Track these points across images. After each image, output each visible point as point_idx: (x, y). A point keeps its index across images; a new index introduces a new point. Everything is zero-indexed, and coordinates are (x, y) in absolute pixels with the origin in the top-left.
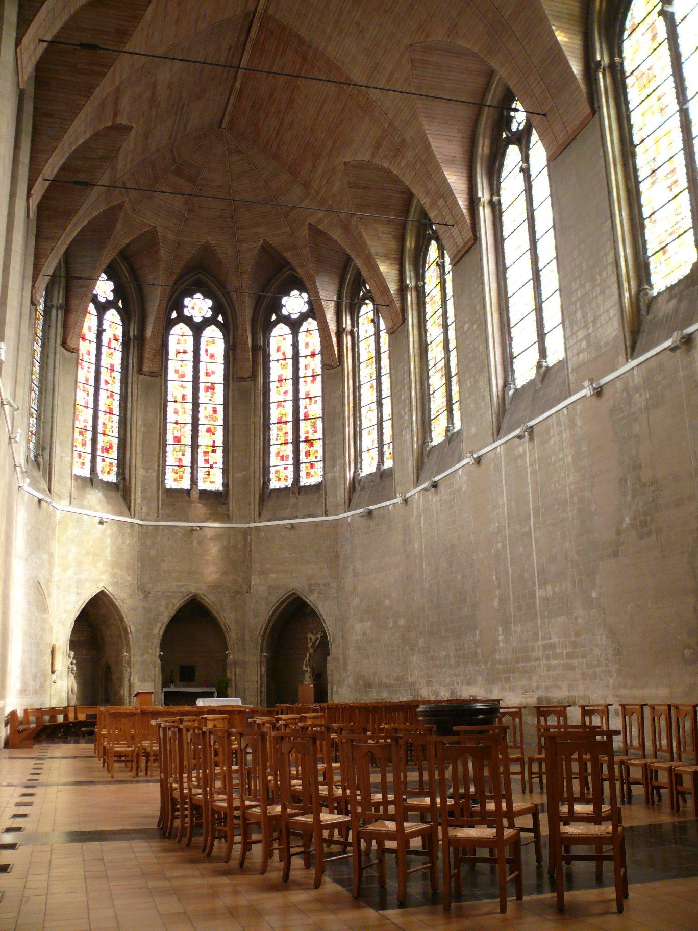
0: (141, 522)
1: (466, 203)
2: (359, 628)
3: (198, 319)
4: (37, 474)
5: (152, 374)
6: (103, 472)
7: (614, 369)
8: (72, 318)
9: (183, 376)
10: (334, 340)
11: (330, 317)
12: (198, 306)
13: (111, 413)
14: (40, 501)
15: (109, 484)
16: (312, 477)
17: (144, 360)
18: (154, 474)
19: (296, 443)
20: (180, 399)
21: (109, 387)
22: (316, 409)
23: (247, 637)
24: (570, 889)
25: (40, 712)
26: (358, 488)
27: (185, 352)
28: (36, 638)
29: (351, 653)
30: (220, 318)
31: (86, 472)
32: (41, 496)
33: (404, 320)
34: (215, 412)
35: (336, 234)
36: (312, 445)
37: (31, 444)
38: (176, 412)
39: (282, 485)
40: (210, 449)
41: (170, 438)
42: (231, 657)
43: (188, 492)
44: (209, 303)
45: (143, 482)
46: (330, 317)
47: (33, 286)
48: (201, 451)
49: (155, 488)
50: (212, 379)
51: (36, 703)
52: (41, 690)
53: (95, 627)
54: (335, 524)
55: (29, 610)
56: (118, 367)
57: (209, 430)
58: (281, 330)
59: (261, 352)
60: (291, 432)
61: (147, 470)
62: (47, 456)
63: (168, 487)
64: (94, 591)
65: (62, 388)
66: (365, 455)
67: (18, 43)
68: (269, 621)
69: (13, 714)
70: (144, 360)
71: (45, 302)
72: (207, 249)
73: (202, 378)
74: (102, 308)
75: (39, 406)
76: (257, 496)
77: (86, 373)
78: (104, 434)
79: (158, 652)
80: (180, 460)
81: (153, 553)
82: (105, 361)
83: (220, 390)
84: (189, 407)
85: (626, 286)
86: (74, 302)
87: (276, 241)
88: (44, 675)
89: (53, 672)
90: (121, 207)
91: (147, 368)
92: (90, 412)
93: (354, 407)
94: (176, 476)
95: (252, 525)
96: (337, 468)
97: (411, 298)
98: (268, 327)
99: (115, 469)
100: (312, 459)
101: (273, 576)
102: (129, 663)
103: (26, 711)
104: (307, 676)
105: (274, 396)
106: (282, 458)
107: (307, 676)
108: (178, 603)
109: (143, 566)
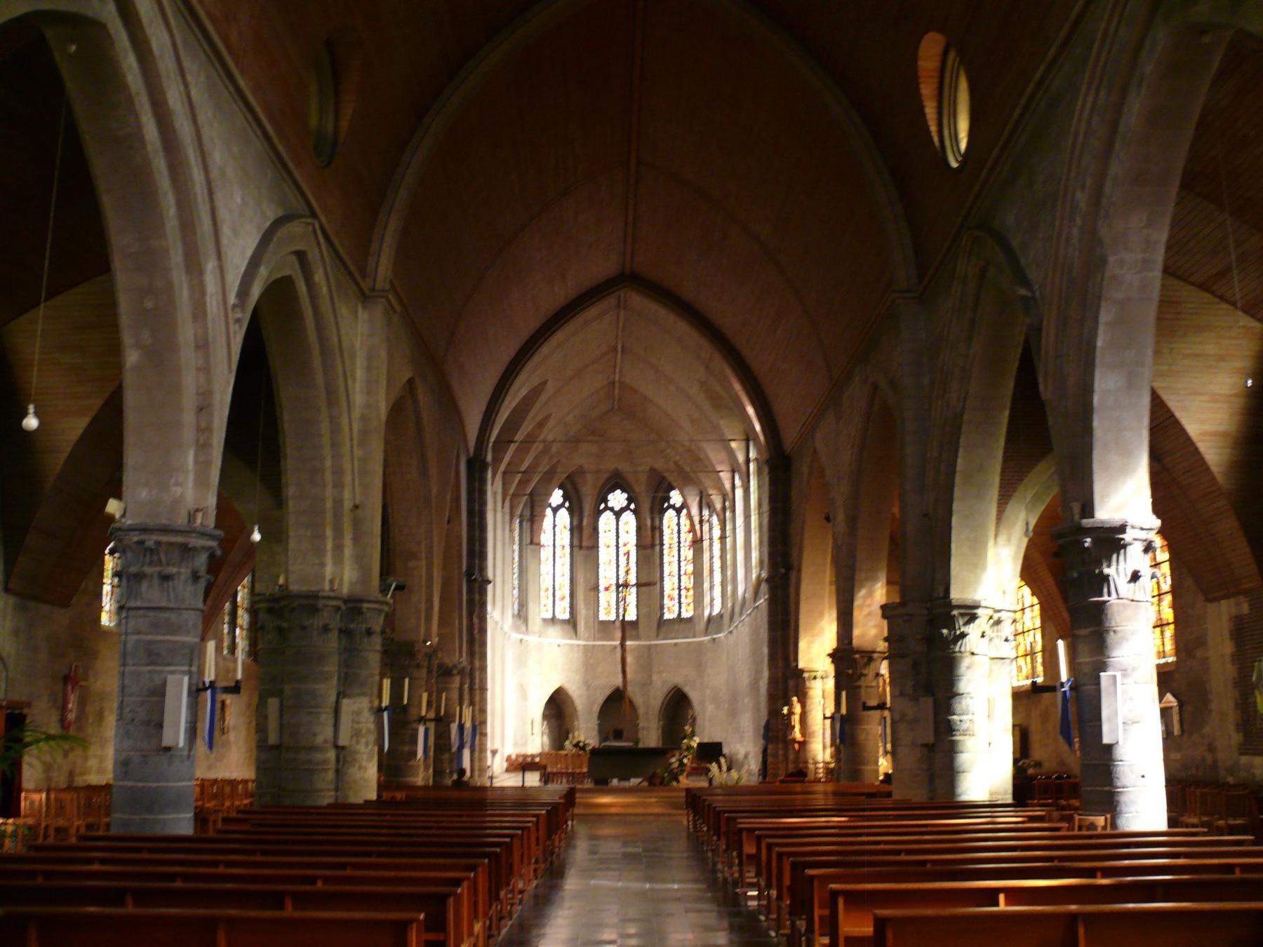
2: (710, 708)
3: (617, 509)
4: (519, 622)
5: (588, 548)
11: (695, 511)
12: (618, 499)
15: (564, 621)
16: (687, 613)
17: (584, 541)
22: (690, 568)
25: (525, 756)
29: (707, 723)
44: (625, 495)
51: (522, 751)
52: (525, 744)
54: (700, 643)
59: (657, 530)
70: (584, 541)
72: (617, 469)
74: (555, 510)
86: (537, 510)
87: (659, 465)
91: (585, 544)
97: (728, 514)
98: (663, 511)
105: (666, 559)
108: (608, 692)
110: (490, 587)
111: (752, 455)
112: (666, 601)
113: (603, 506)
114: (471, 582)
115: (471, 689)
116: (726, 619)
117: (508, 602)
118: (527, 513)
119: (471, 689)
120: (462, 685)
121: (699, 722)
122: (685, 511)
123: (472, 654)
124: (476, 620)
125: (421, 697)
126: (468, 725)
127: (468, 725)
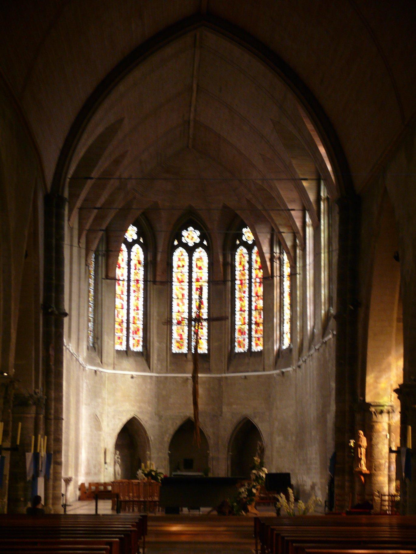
0: (157, 375)
1: (301, 224)
2: (278, 439)
3: (191, 244)
4: (94, 355)
5: (162, 283)
6: (134, 346)
8: (111, 261)
10: (268, 264)
11: (266, 249)
12: (191, 236)
15: (138, 353)
16: (257, 348)
18: (165, 345)
19: (250, 324)
20: (180, 297)
23: (220, 442)
25: (98, 485)
26: (281, 355)
28: (94, 447)
29: (275, 454)
31: (123, 348)
32: (95, 368)
37: (91, 337)
38: (178, 305)
42: (211, 454)
45: (158, 351)
46: (266, 249)
47: (86, 260)
49: (165, 354)
51: (95, 479)
52: (98, 473)
53: (130, 438)
54: (270, 377)
56: (141, 308)
61: (160, 343)
63: (174, 352)
64: (124, 419)
65: (106, 303)
66: (285, 336)
68: (233, 434)
69: (83, 485)
70: (158, 277)
75: (94, 315)
76: (226, 357)
77: (120, 288)
78: (134, 323)
79: (168, 451)
80: (181, 335)
81: (164, 393)
84: (186, 301)
88: (100, 464)
89: (105, 463)
91: (158, 279)
92: (125, 311)
93: (280, 306)
94: (178, 345)
95: (224, 375)
96: (270, 343)
99: (141, 343)
101: (234, 406)
102: (150, 458)
103: (90, 484)
108: (179, 423)
110: (66, 320)
111: (323, 194)
112: (237, 335)
114: (47, 315)
116: (295, 353)
117: (84, 335)
118: (103, 248)
120: (37, 414)
121: (267, 453)
122: (255, 249)
123: (47, 384)
124: (52, 352)
126: (43, 453)
127: (43, 453)
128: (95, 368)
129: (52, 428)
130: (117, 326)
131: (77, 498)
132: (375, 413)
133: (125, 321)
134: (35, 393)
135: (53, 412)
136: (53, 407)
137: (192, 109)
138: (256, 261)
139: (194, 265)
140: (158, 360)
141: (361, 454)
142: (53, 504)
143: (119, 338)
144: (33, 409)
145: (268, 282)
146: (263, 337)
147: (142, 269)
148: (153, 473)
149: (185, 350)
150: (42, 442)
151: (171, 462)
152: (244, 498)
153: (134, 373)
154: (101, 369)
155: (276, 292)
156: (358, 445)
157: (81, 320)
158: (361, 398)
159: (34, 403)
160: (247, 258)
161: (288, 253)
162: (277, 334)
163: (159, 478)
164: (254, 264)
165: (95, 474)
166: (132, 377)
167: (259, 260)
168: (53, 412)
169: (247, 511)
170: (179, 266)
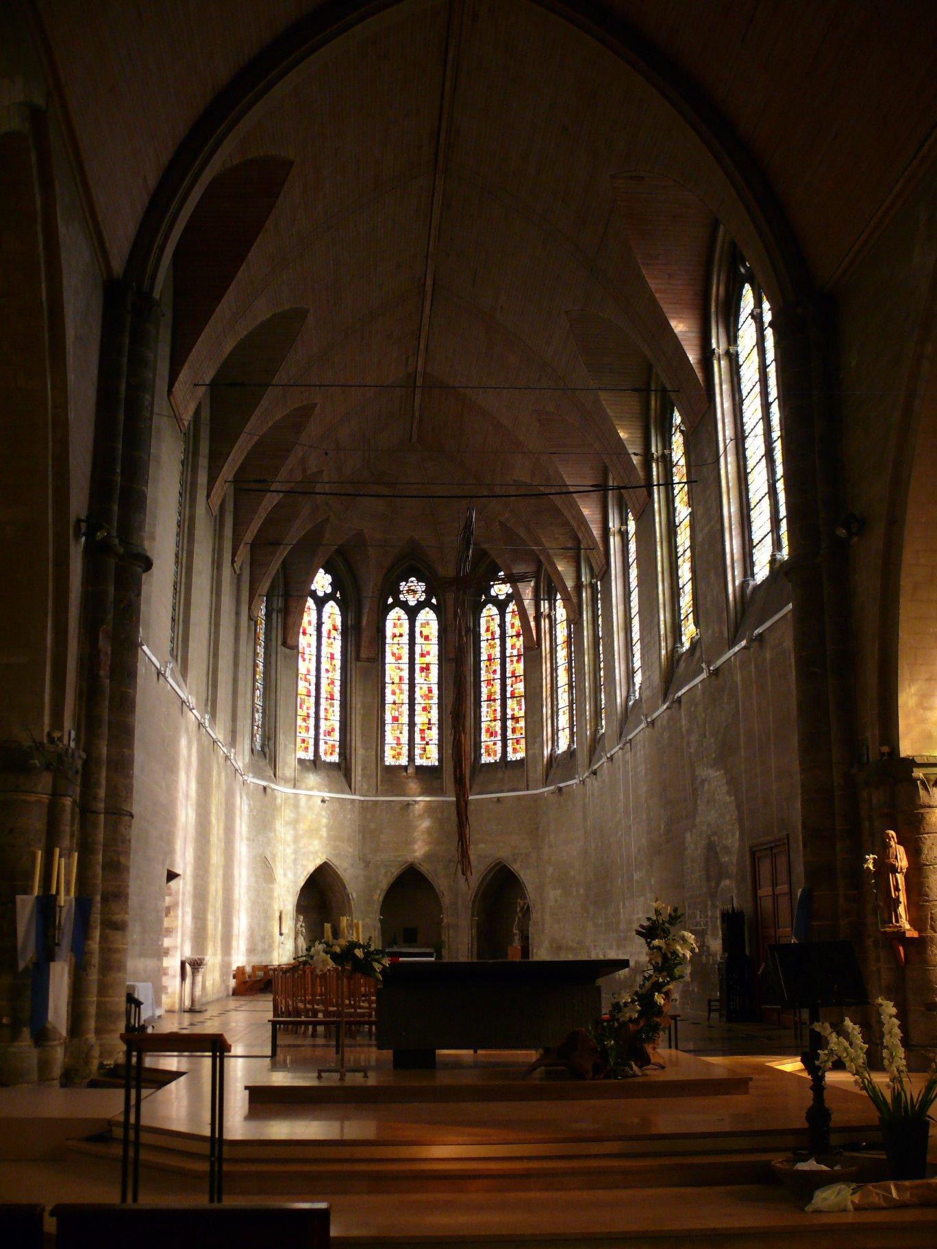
2: (553, 895)
4: (263, 763)
5: (368, 660)
7: (657, 709)
8: (291, 620)
9: (400, 658)
10: (533, 624)
11: (528, 603)
12: (413, 590)
13: (332, 699)
14: (265, 788)
16: (517, 754)
19: (504, 720)
20: (397, 680)
21: (330, 675)
23: (460, 903)
24: (142, 955)
26: (554, 765)
27: (401, 635)
28: (261, 907)
29: (547, 917)
30: (434, 601)
31: (310, 756)
32: (264, 783)
33: (581, 614)
34: (430, 691)
35: (522, 532)
36: (517, 722)
39: (491, 760)
40: (425, 727)
41: (388, 718)
43: (405, 768)
46: (528, 603)
47: (250, 608)
48: (417, 729)
50: (427, 659)
51: (259, 960)
52: (268, 950)
53: (320, 895)
54: (536, 798)
55: (257, 882)
56: (338, 656)
57: (424, 709)
58: (491, 610)
60: (499, 709)
61: (366, 749)
62: (272, 746)
63: (387, 763)
65: (283, 684)
67: (208, 496)
71: (267, 607)
73: (418, 659)
74: (321, 602)
75: (264, 702)
79: (378, 916)
80: (398, 738)
81: (372, 826)
82: (325, 651)
83: (434, 670)
84: (406, 687)
85: (663, 644)
89: (281, 934)
90: (327, 519)
91: (363, 655)
93: (552, 688)
96: (537, 745)
98: (479, 608)
99: (337, 750)
100: (517, 735)
101: (481, 846)
103: (254, 967)
104: (517, 938)
106: (491, 735)
107: (517, 938)
108: (395, 872)
109: (364, 838)
112: (484, 737)
113: (390, 600)
114: (95, 552)
115: (85, 810)
116: (582, 757)
117: (244, 726)
119: (85, 810)
120: (56, 794)
121: (535, 916)
122: (512, 607)
123: (89, 724)
124: (104, 645)
125: (34, 856)
126: (66, 899)
127: (66, 899)
128: (264, 783)
129: (101, 836)
130: (300, 721)
131: (231, 992)
132: (923, 783)
133: (312, 715)
134: (51, 740)
135: (102, 793)
136: (103, 782)
137: (417, 414)
138: (513, 626)
139: (417, 635)
140: (363, 776)
141: (897, 889)
142: (98, 1032)
143: (303, 741)
144: (45, 781)
145: (533, 653)
146: (526, 738)
147: (339, 637)
148: (359, 953)
149: (404, 761)
150: (66, 868)
151: (384, 932)
152: (630, 1020)
153: (327, 795)
154: (273, 786)
155: (546, 667)
156: (886, 867)
157: (240, 703)
158: (885, 749)
159: (48, 767)
160: (497, 620)
161: (567, 600)
162: (547, 731)
163: (376, 966)
164: (510, 631)
165: (264, 951)
166: (323, 801)
167: (517, 622)
168: (102, 793)
169: (644, 1060)
170: (394, 636)
